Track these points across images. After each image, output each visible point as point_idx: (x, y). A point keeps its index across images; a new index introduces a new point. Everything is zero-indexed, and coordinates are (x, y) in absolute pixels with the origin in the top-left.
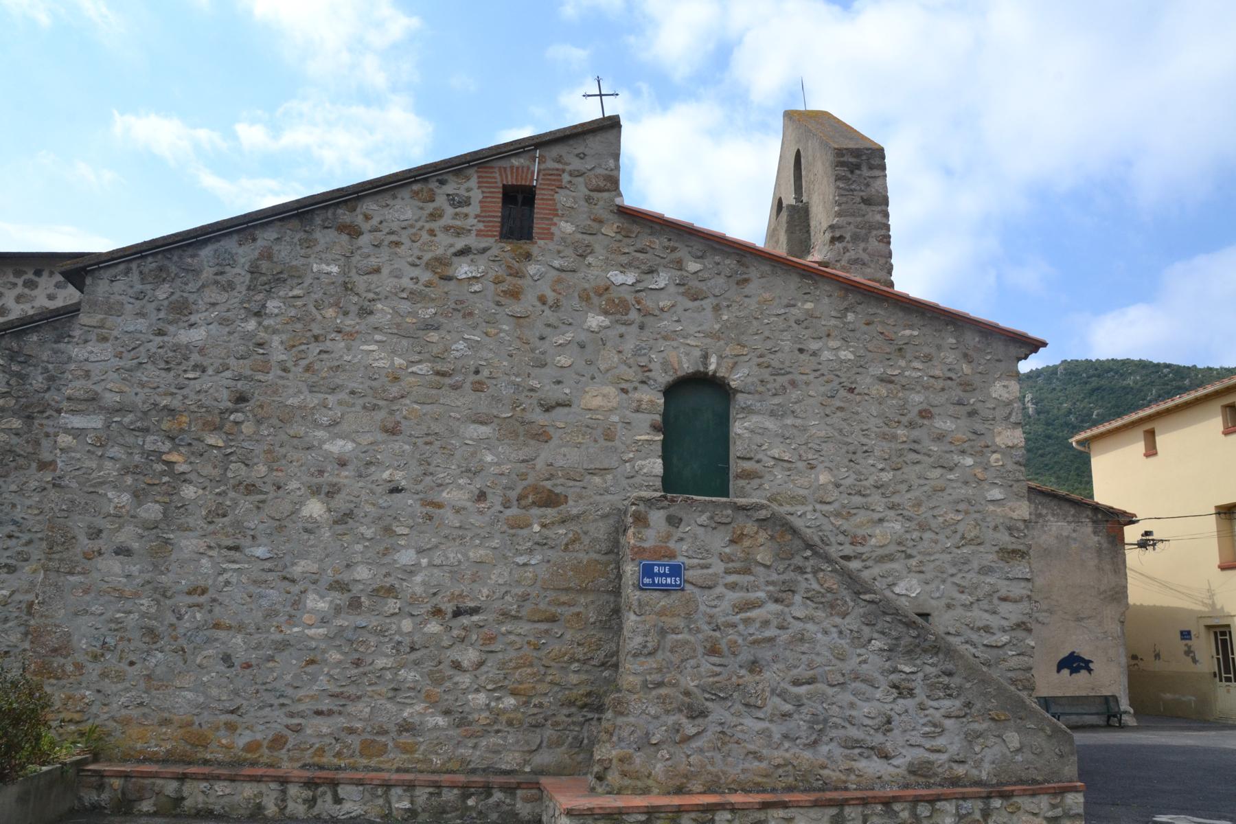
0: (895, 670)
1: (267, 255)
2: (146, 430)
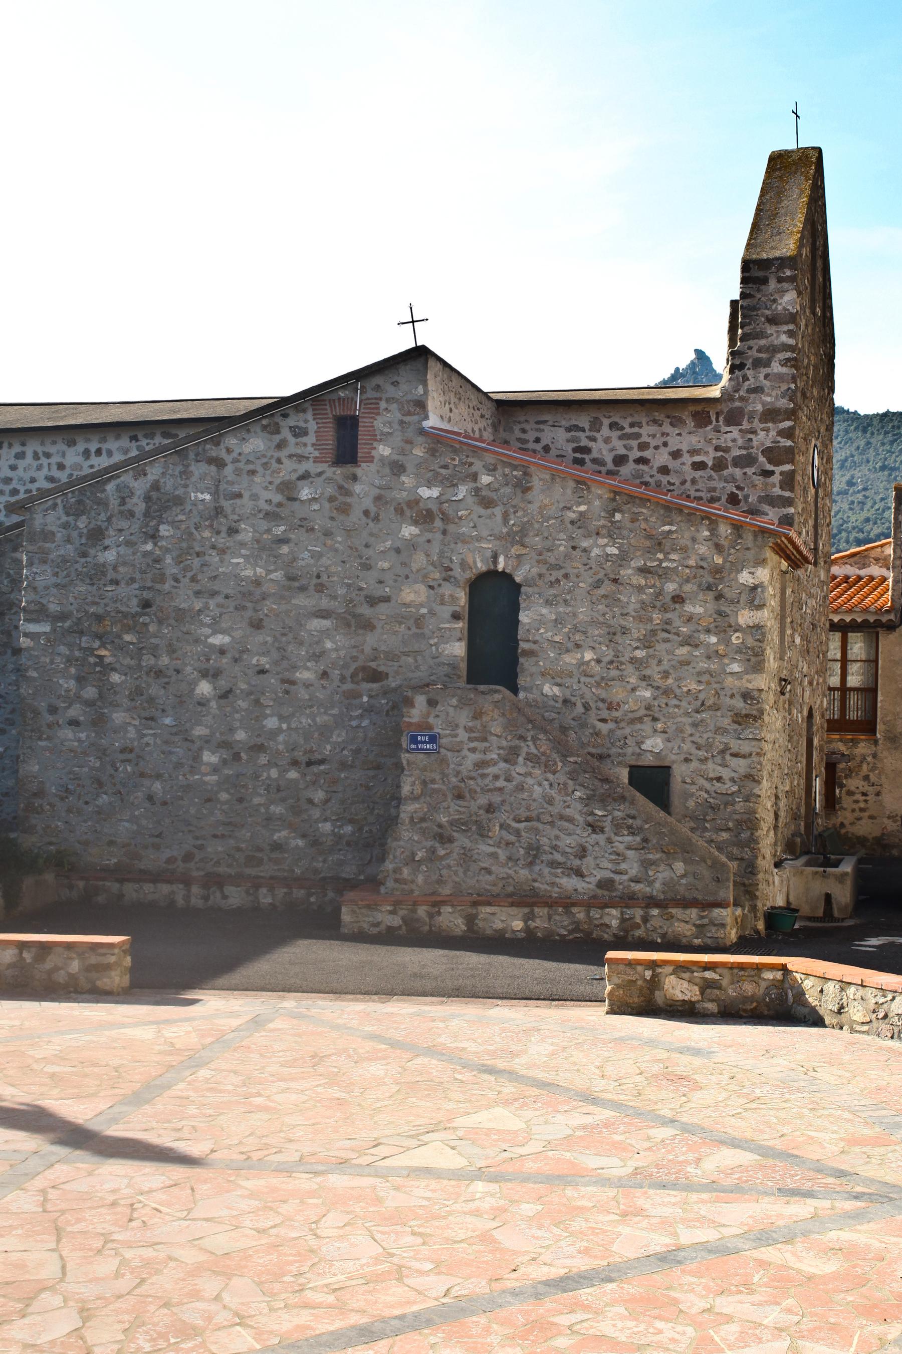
0: (592, 814)
1: (156, 486)
2: (82, 633)
